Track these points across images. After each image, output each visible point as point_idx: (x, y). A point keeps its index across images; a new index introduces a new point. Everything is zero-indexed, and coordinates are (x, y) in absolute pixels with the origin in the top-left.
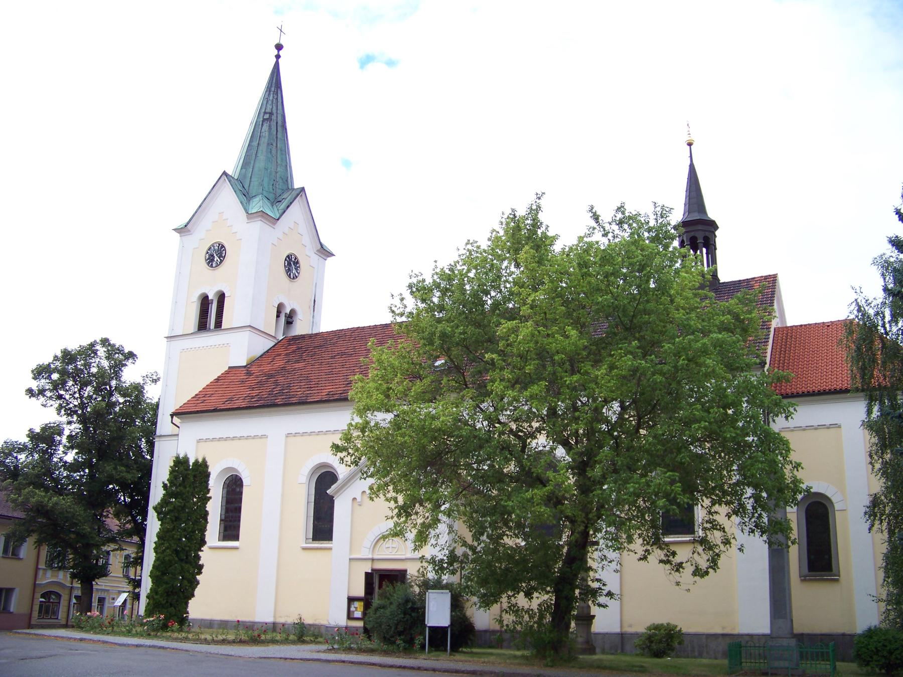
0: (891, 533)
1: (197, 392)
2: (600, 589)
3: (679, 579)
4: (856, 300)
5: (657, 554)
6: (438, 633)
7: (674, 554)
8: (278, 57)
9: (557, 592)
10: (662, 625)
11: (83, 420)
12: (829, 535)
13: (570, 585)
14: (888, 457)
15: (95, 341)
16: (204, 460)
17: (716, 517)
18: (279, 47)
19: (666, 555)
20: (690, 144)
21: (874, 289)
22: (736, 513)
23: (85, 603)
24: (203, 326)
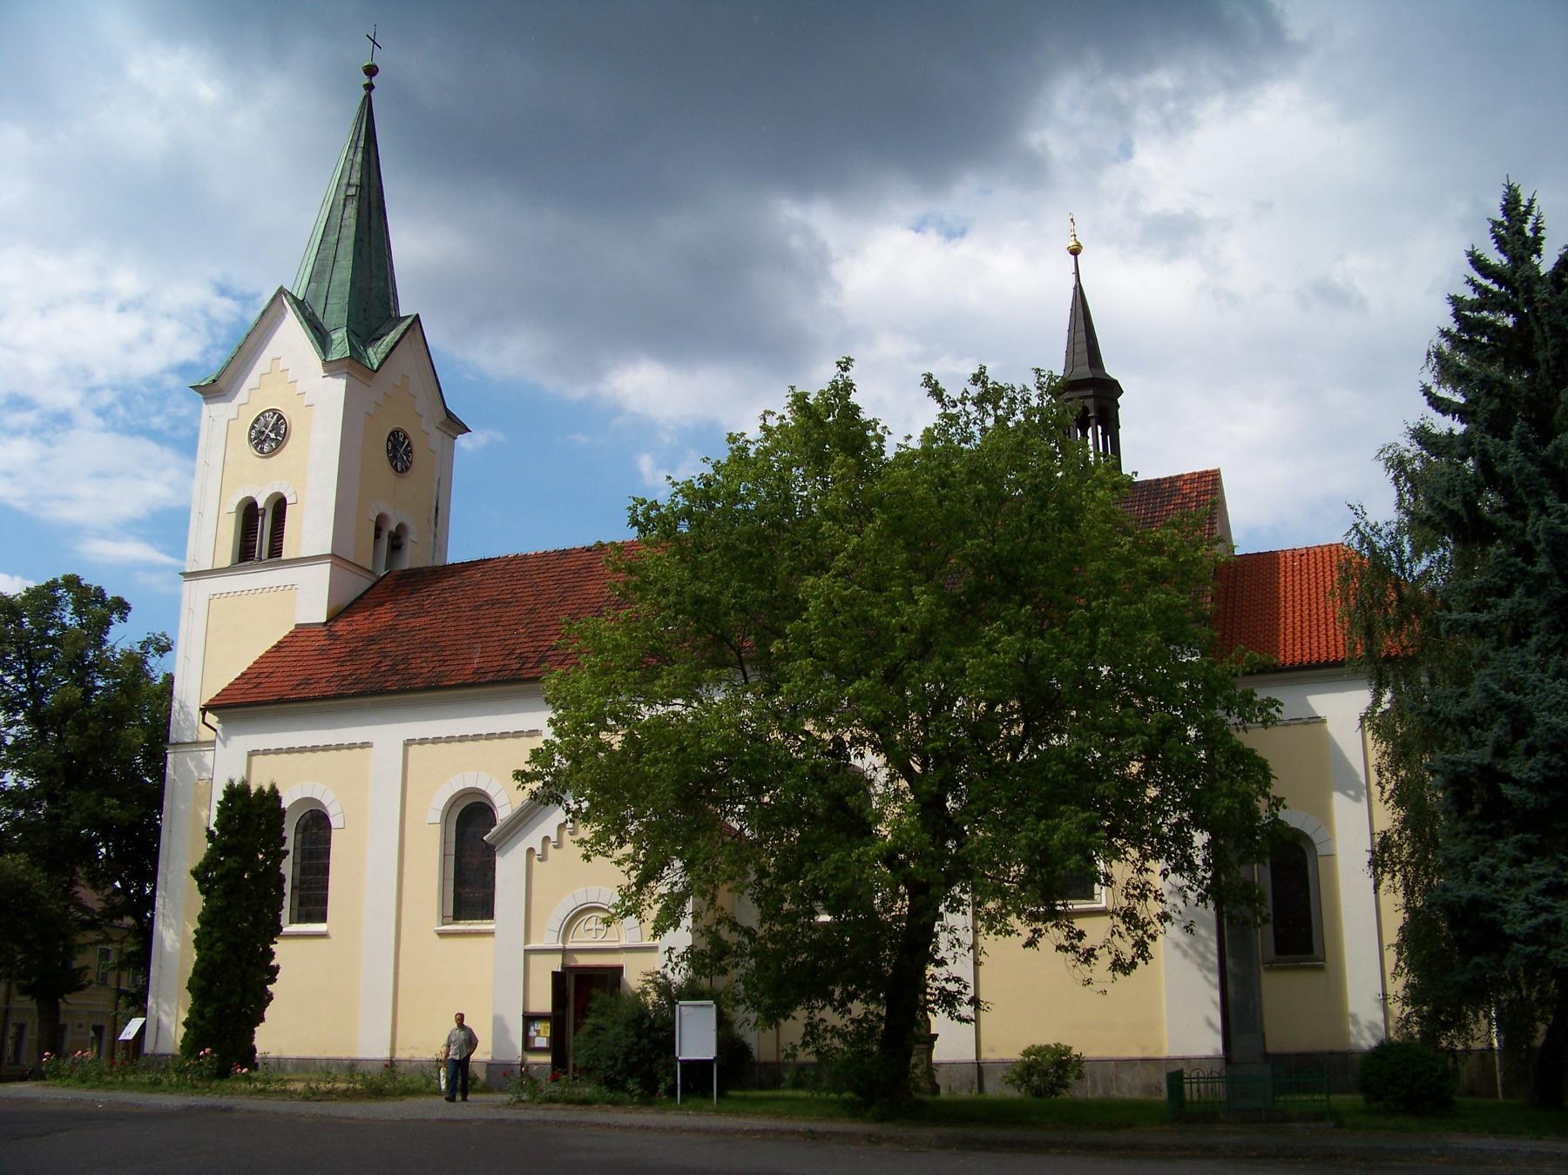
0: (1409, 892)
1: (244, 669)
2: (960, 992)
3: (1088, 975)
4: (1356, 526)
5: (1054, 934)
6: (696, 1070)
7: (1081, 935)
8: (369, 87)
9: (891, 1003)
10: (1048, 1047)
11: (34, 718)
12: (1308, 898)
13: (905, 992)
14: (1403, 773)
15: (55, 581)
16: (273, 787)
17: (1145, 876)
18: (371, 71)
19: (1068, 937)
20: (1075, 252)
21: (1384, 507)
22: (1177, 869)
23: (54, 1039)
24: (246, 553)
